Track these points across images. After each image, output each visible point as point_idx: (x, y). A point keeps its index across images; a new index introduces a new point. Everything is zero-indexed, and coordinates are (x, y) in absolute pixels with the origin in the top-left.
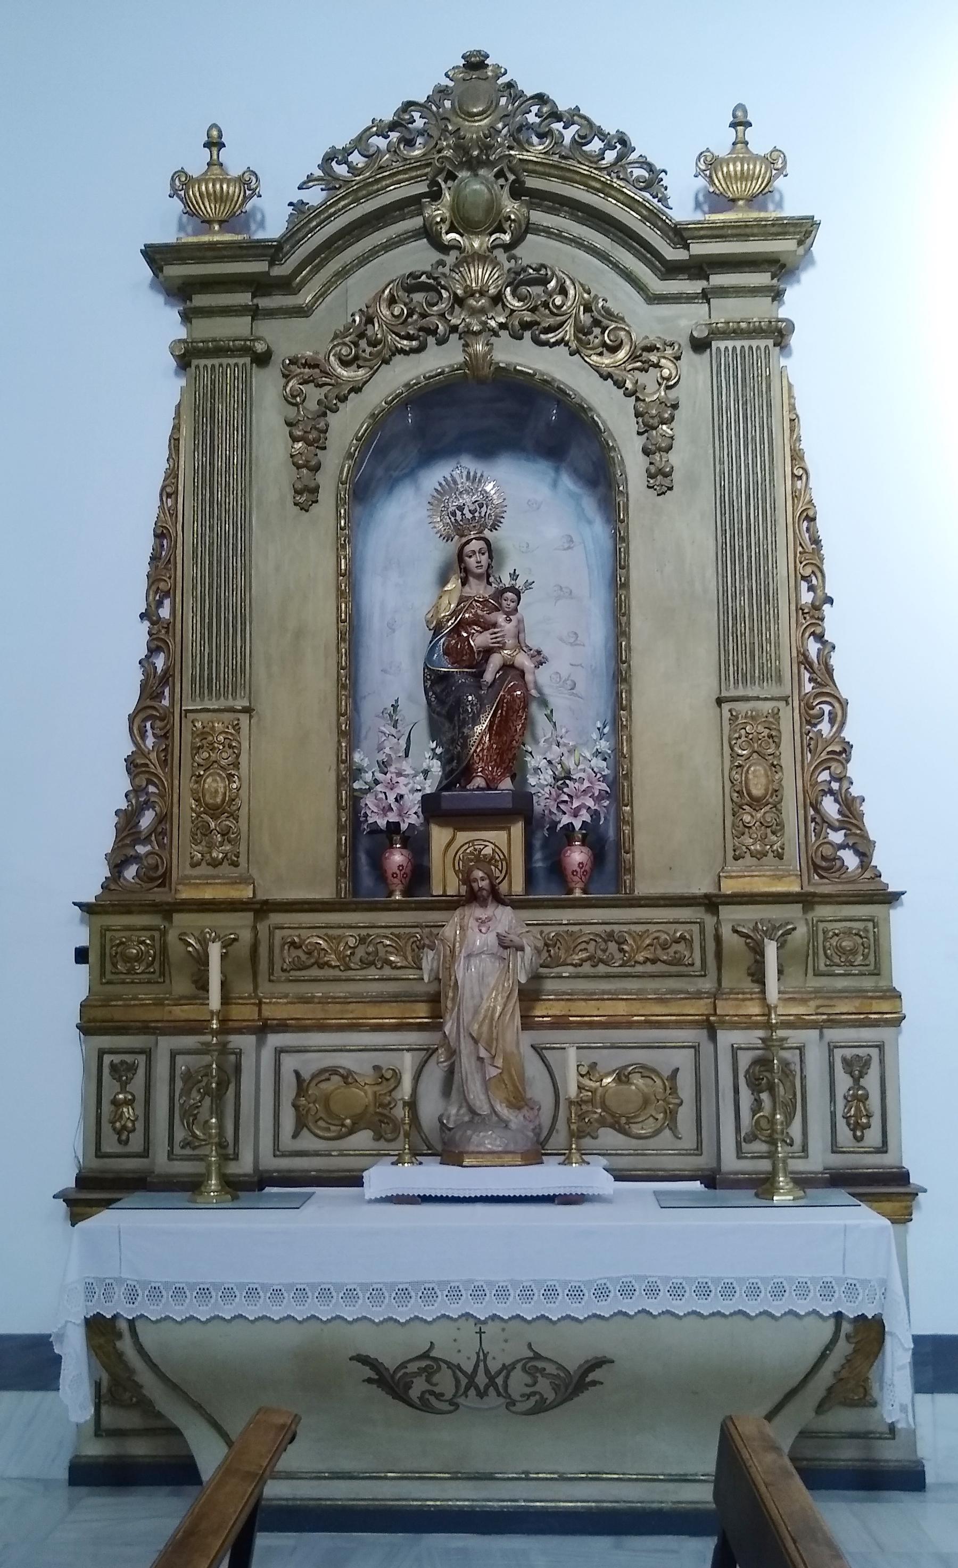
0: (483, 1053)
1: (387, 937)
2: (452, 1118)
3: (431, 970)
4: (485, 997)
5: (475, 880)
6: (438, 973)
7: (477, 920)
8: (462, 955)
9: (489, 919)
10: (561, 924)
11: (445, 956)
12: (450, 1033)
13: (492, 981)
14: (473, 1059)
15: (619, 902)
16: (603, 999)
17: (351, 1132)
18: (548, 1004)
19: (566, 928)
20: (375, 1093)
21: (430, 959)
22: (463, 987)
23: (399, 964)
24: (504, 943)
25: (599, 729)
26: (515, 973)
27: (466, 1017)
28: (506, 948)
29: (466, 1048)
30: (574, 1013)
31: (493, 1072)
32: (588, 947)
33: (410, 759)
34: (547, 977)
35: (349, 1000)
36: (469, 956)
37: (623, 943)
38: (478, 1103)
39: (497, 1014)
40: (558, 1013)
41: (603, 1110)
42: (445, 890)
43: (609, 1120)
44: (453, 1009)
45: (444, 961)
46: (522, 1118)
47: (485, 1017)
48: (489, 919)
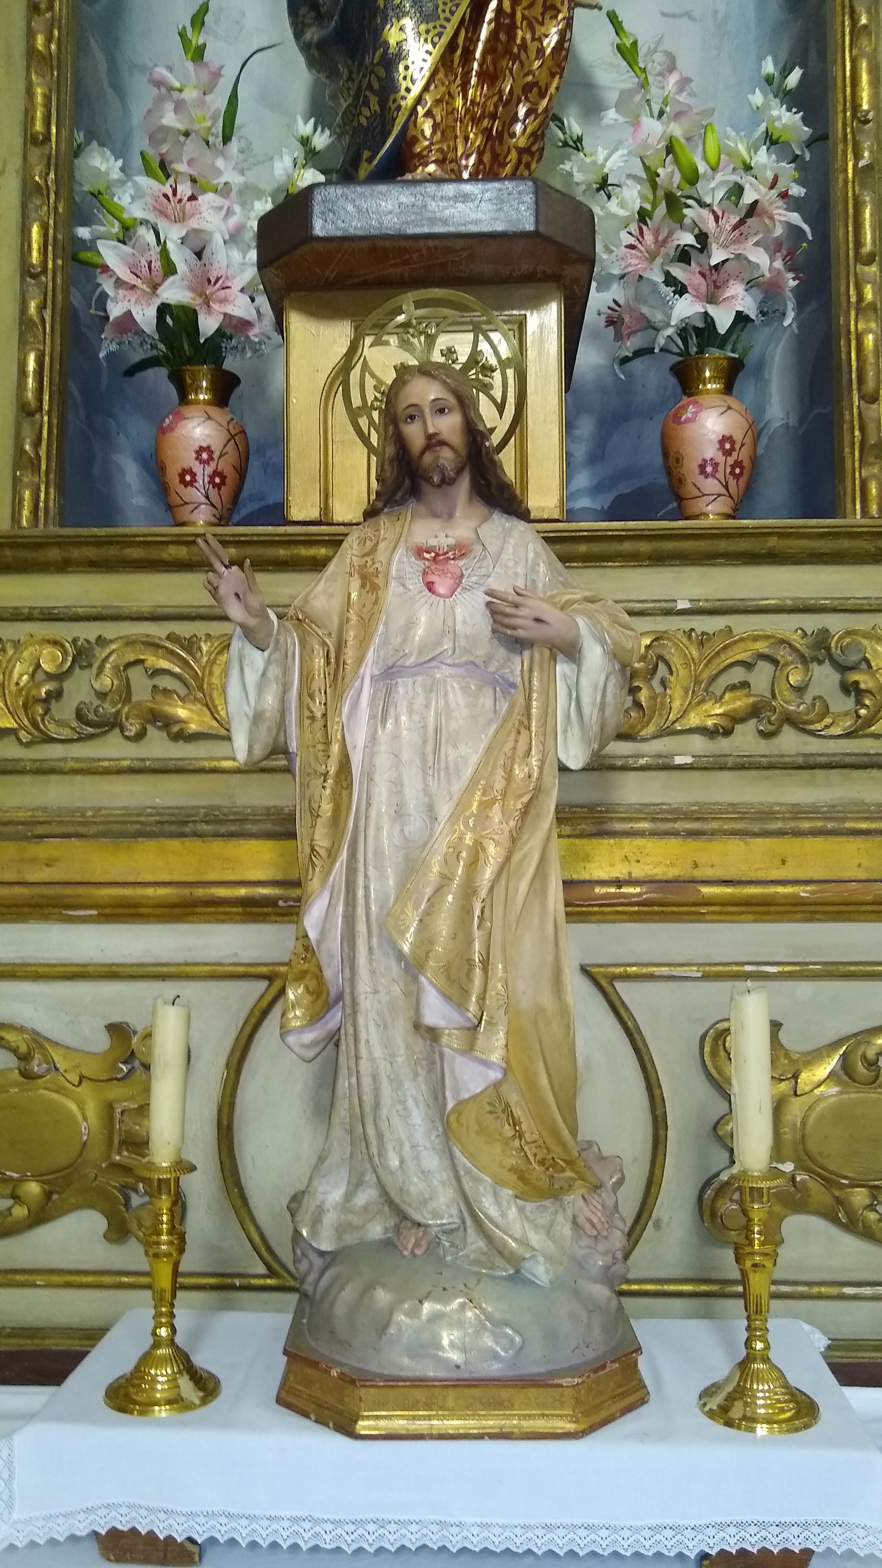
0: (436, 1011)
1: (153, 645)
2: (330, 1219)
3: (257, 718)
4: (444, 811)
5: (414, 414)
6: (282, 724)
7: (419, 552)
8: (369, 669)
9: (461, 551)
10: (669, 612)
11: (306, 678)
12: (323, 932)
13: (468, 754)
14: (400, 1032)
15: (845, 544)
16: (797, 833)
17: (40, 1216)
18: (629, 845)
19: (686, 623)
20: (109, 1107)
21: (252, 678)
22: (369, 777)
23: (193, 727)
24: (509, 627)
25: (769, 80)
26: (549, 734)
27: (380, 882)
28: (518, 645)
29: (375, 989)
30: (710, 873)
31: (471, 1078)
32: (752, 678)
33: (234, 145)
34: (624, 768)
35: (39, 830)
36: (389, 674)
37: (853, 668)
38: (416, 1186)
39: (488, 873)
40: (659, 872)
41: (801, 1166)
42: (326, 508)
43: (818, 1193)
44: (332, 854)
45: (306, 692)
46: (567, 1230)
47: (445, 879)
48: (461, 551)
